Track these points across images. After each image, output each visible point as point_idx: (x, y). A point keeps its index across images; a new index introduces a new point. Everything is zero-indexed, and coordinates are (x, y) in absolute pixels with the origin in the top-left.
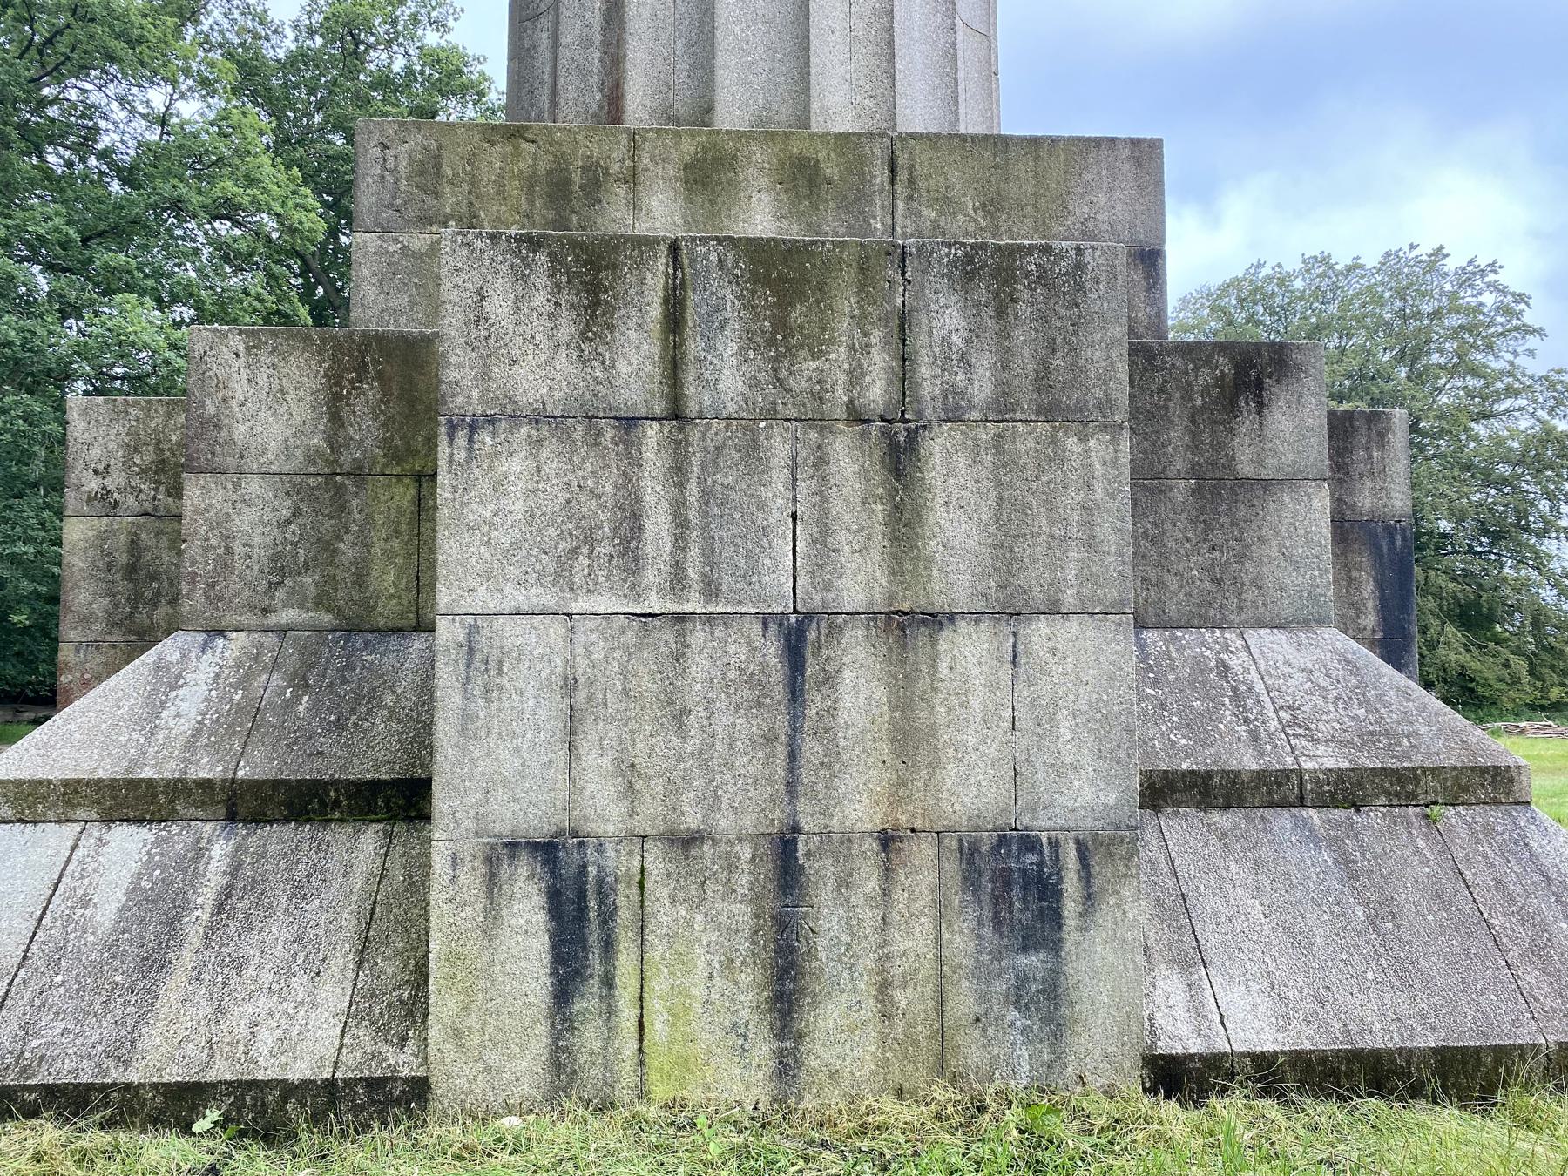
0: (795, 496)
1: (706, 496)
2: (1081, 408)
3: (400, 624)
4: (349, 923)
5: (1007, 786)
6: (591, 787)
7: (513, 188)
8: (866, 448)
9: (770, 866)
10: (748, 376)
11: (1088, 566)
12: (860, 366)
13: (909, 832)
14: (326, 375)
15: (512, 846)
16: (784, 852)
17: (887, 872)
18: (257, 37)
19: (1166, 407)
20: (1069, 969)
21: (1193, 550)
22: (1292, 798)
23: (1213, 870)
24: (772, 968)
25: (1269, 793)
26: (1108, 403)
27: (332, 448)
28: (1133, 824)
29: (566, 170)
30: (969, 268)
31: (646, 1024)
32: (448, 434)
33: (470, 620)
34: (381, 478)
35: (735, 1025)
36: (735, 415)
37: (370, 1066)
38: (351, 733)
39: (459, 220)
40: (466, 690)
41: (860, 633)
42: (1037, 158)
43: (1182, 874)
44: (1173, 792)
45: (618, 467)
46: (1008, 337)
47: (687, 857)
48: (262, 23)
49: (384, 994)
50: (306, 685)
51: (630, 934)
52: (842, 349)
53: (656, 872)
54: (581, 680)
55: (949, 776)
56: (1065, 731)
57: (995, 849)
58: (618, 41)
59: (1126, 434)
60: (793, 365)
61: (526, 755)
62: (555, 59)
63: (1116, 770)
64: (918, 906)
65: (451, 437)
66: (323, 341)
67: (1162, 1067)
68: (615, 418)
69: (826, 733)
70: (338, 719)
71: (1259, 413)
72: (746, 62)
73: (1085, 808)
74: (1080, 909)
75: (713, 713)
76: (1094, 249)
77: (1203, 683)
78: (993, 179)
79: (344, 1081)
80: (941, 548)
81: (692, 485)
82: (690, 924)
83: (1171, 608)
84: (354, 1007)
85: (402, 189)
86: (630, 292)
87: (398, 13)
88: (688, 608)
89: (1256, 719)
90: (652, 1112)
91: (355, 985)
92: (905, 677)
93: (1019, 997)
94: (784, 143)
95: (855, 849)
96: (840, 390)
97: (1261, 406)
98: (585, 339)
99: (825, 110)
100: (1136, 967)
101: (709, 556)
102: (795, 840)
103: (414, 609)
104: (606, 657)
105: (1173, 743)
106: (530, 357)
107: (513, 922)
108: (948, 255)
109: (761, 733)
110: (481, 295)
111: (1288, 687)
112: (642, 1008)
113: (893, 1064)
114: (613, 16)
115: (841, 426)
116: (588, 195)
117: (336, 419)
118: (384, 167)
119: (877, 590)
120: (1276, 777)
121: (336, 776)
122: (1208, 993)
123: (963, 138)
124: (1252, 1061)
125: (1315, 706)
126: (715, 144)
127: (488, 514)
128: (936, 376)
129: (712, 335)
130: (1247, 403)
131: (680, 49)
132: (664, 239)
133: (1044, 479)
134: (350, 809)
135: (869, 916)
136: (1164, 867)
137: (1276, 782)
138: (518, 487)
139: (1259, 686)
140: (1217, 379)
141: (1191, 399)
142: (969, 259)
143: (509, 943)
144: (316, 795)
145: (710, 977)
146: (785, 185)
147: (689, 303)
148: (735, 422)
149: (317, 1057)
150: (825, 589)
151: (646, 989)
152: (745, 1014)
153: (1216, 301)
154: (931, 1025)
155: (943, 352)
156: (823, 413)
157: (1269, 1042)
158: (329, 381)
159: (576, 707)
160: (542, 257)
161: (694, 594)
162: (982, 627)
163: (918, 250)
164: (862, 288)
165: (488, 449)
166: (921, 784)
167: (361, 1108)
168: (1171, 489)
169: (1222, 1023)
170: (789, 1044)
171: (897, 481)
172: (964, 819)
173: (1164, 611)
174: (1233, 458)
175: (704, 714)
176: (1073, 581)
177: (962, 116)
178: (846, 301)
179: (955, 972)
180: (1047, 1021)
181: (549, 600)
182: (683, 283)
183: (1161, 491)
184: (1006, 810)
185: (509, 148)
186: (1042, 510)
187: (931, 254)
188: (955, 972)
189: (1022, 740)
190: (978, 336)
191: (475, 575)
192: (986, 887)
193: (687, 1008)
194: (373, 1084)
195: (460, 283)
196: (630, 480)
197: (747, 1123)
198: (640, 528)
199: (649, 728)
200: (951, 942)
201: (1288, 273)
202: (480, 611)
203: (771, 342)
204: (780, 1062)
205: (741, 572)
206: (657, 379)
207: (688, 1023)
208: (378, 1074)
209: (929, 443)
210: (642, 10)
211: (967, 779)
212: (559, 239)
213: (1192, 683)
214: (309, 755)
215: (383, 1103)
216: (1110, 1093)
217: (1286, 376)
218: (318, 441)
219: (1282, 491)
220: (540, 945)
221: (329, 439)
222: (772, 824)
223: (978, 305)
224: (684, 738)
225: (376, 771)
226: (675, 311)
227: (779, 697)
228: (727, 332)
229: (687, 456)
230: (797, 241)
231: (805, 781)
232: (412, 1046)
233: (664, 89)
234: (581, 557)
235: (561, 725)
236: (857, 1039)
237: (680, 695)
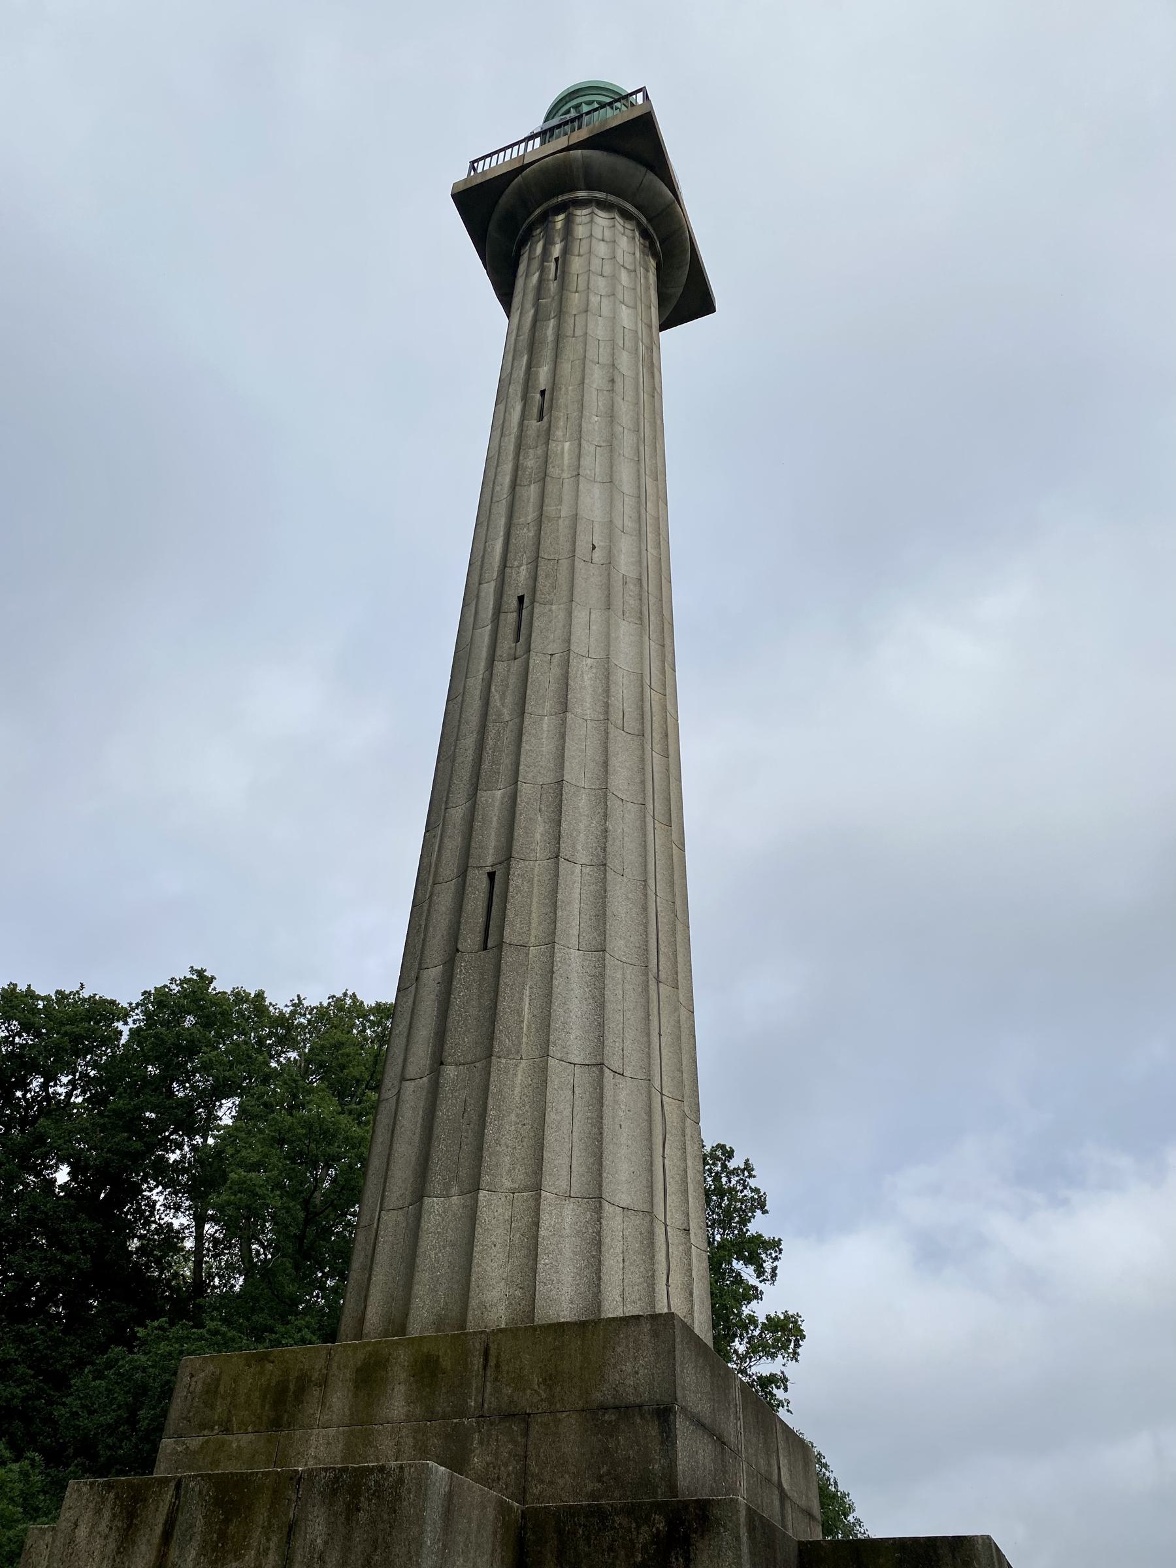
52: (253, 1552)
85: (196, 1404)
98: (118, 1552)
99: (483, 1306)
108: (324, 1478)
118: (189, 1392)
129: (184, 1546)
130: (677, 1559)
182: (177, 1509)
210: (385, 1246)
223: (335, 1515)
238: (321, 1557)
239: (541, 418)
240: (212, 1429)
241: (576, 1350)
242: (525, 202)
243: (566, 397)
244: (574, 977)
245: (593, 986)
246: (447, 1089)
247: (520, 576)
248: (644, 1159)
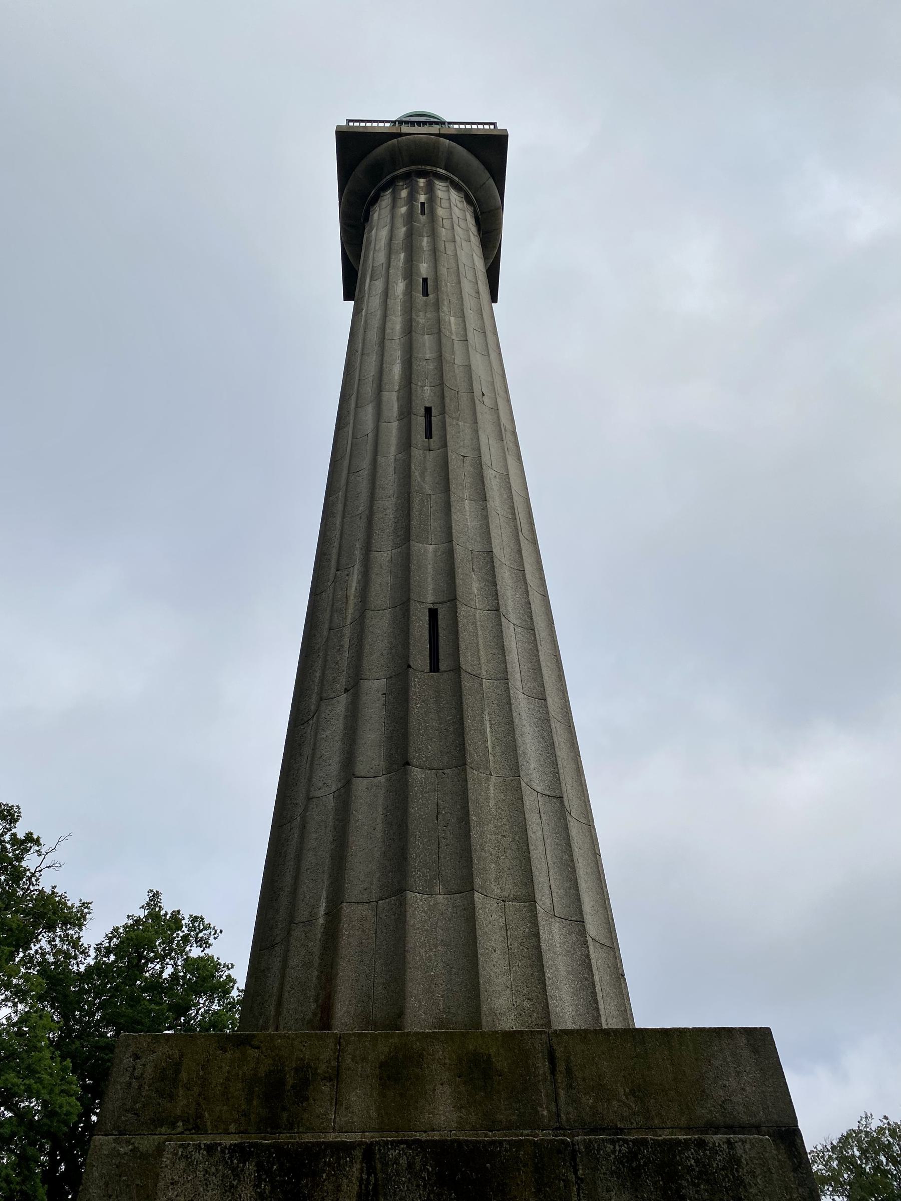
18: (67, 956)
30: (634, 1165)
39: (186, 1121)
62: (283, 977)
76: (744, 1142)
108: (614, 1152)
118: (132, 1076)
123: (607, 1032)
142: (633, 1156)
160: (250, 1167)
163: (586, 1148)
177: (602, 1012)
187: (598, 1151)
239: (426, 293)
240: (173, 1125)
241: (663, 1059)
242: (394, 159)
243: (448, 286)
244: (524, 715)
245: (540, 727)
246: (416, 788)
247: (426, 394)
248: (598, 897)
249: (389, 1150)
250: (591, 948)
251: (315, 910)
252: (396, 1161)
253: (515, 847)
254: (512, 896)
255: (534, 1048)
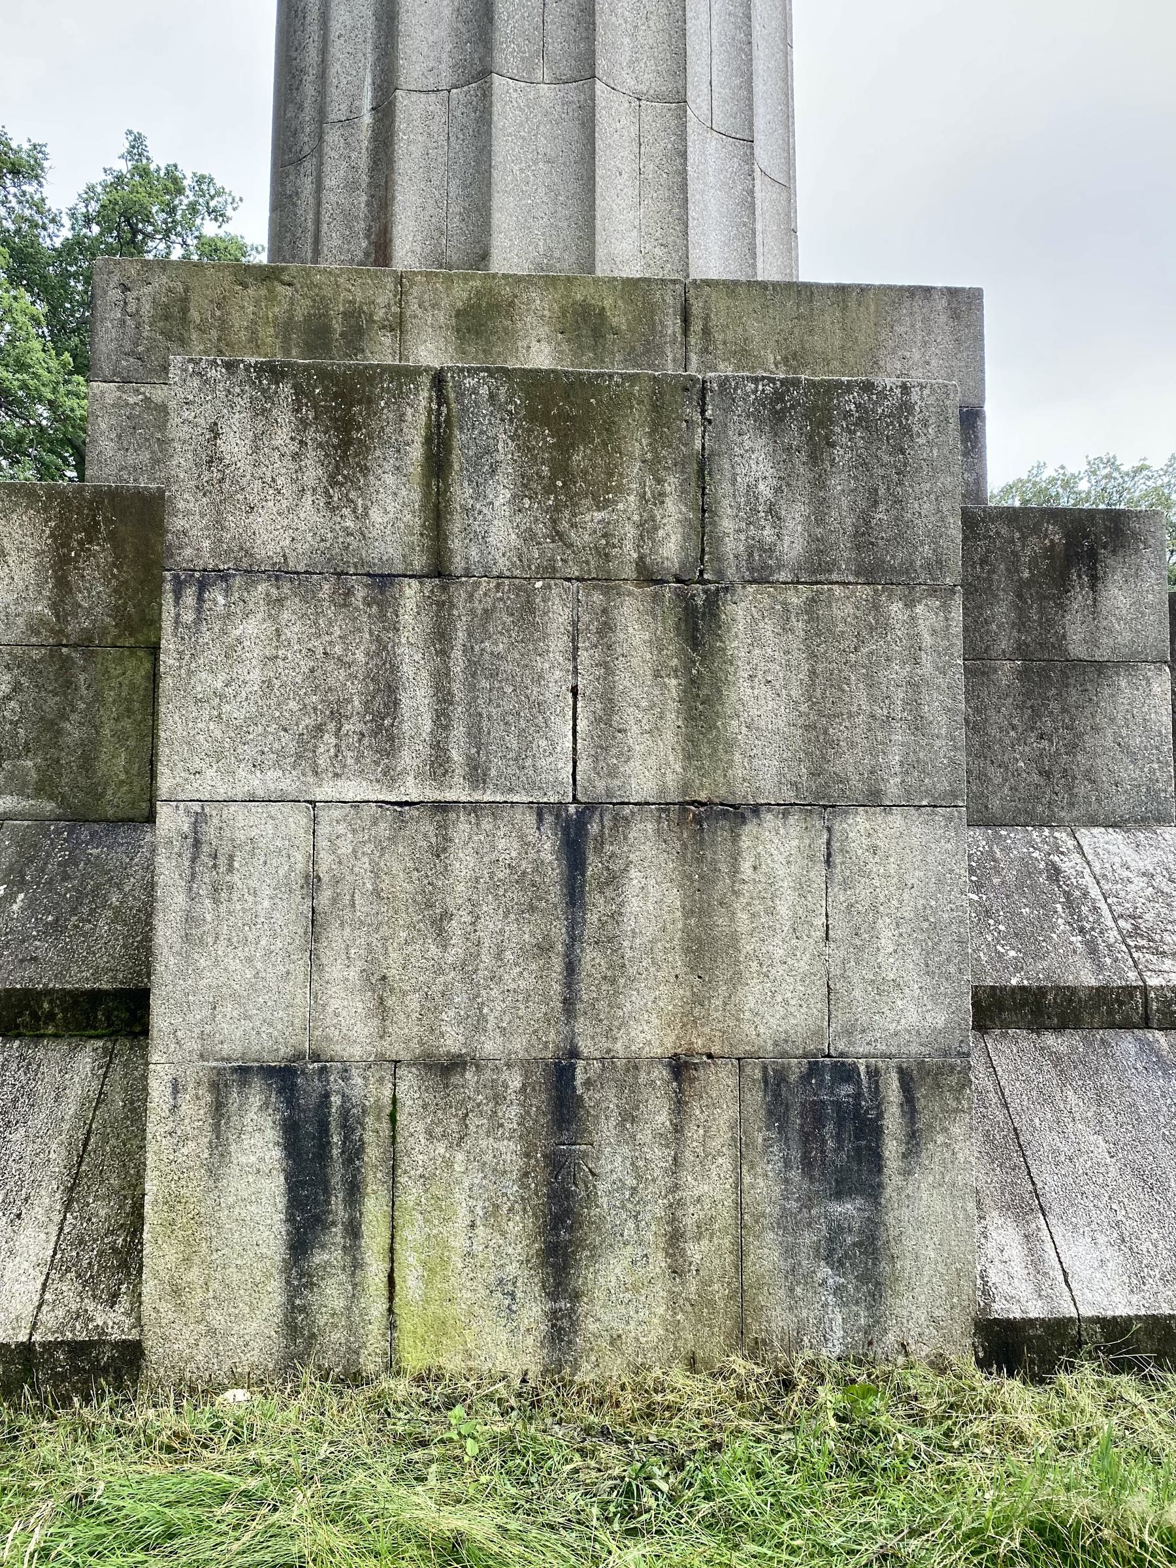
0: (575, 667)
1: (473, 667)
2: (907, 569)
3: (131, 814)
4: (57, 1156)
5: (819, 1006)
6: (335, 1004)
7: (267, 334)
8: (659, 612)
9: (544, 1096)
10: (523, 527)
11: (915, 752)
12: (652, 518)
13: (705, 1058)
14: (52, 535)
15: (243, 1072)
16: (559, 1079)
17: (680, 1106)
19: (989, 580)
20: (890, 1219)
21: (1019, 739)
22: (1136, 1019)
23: (1049, 1100)
24: (545, 1216)
25: (1110, 1012)
26: (938, 564)
27: (57, 616)
28: (965, 1050)
29: (326, 315)
30: (778, 407)
31: (397, 1280)
32: (174, 591)
33: (196, 807)
34: (112, 650)
35: (501, 1281)
36: (508, 574)
37: (73, 1329)
38: (70, 936)
40: (190, 889)
41: (649, 826)
42: (845, 309)
43: (1014, 1105)
44: (1001, 1010)
45: (371, 633)
46: (823, 487)
47: (447, 1086)
48: (38, 212)
49: (95, 1240)
50: (23, 882)
51: (379, 1175)
52: (632, 498)
53: (410, 1103)
54: (325, 878)
55: (751, 995)
56: (887, 941)
57: (805, 1078)
58: (386, 182)
59: (958, 600)
60: (575, 515)
61: (259, 965)
62: (319, 204)
63: (945, 987)
64: (716, 1144)
65: (178, 596)
66: (50, 497)
67: (998, 1333)
68: (368, 575)
69: (609, 942)
70: (57, 920)
71: (1093, 587)
72: (526, 205)
73: (909, 1032)
74: (903, 1149)
75: (478, 917)
77: (1032, 888)
78: (796, 330)
79: (42, 1345)
80: (744, 730)
81: (457, 653)
82: (449, 1164)
83: (995, 804)
84: (58, 1256)
85: (145, 334)
86: (388, 430)
87: (177, 202)
88: (450, 796)
89: (1093, 929)
90: (401, 1388)
91: (61, 1229)
92: (702, 877)
93: (831, 1251)
94: (566, 289)
95: (643, 1077)
96: (628, 546)
97: (1094, 580)
98: (333, 482)
100: (967, 1217)
101: (475, 736)
102: (573, 1067)
103: (147, 797)
104: (354, 851)
105: (1000, 956)
106: (271, 504)
107: (243, 1160)
108: (755, 392)
109: (534, 941)
110: (215, 432)
111: (1127, 893)
112: (392, 1261)
113: (684, 1329)
114: (382, 155)
115: (630, 587)
116: (349, 343)
117: (63, 585)
118: (124, 311)
119: (670, 777)
120: (1118, 994)
121: (51, 986)
122: (1049, 1246)
123: (764, 286)
124: (1102, 1328)
125: (1158, 915)
126: (491, 289)
127: (219, 685)
128: (739, 531)
130: (1079, 577)
131: (454, 190)
132: (427, 369)
133: (865, 650)
134: (66, 1022)
135: (659, 1156)
136: (993, 1098)
137: (1117, 1000)
138: (253, 653)
139: (1094, 892)
140: (1046, 549)
141: (1018, 571)
142: (778, 397)
143: (236, 1185)
144: (27, 1006)
145: (473, 1226)
146: (567, 335)
147: (455, 444)
148: (507, 582)
149: (13, 1316)
150: (609, 775)
151: (397, 1239)
152: (512, 1269)
153: (1008, 490)
154: (729, 1284)
155: (748, 503)
156: (609, 572)
157: (1121, 1306)
158: (55, 542)
159: (319, 909)
160: (286, 389)
161: (458, 779)
162: (792, 820)
163: (720, 386)
164: (655, 428)
165: (220, 609)
166: (719, 1002)
167: (63, 1377)
168: (995, 671)
169: (1066, 1281)
170: (564, 1304)
171: (694, 650)
172: (770, 1042)
173: (986, 807)
174: (1064, 637)
175: (468, 919)
176: (898, 769)
178: (637, 443)
179: (757, 1222)
180: (863, 1279)
181: (288, 784)
183: (983, 673)
184: (818, 1033)
185: (263, 292)
186: (861, 686)
187: (735, 389)
188: (757, 1222)
189: (836, 952)
190: (788, 485)
191: (203, 755)
192: (794, 1123)
193: (444, 1262)
194: (77, 1349)
195: (191, 418)
196: (385, 648)
197: (513, 1402)
198: (396, 703)
199: (403, 935)
200: (752, 1186)
201: (1073, 475)
202: (208, 797)
203: (550, 489)
204: (553, 1326)
205: (511, 755)
206: (417, 530)
207: (446, 1279)
208: (83, 1337)
209: (730, 607)
210: (412, 148)
211: (773, 997)
212: (306, 368)
213: (1020, 887)
214: (22, 961)
215: (89, 1371)
216: (940, 1366)
217: (1123, 546)
218: (42, 608)
219: (1118, 675)
220: (274, 1187)
221: (54, 606)
222: (546, 1047)
223: (788, 449)
224: (444, 946)
225: (97, 980)
226: (439, 452)
227: (556, 900)
228: (499, 477)
229: (451, 621)
230: (580, 374)
231: (585, 997)
232: (124, 1302)
233: (436, 234)
234: (326, 736)
235: (301, 931)
236: (643, 1299)
237: (440, 896)
238: (771, 510)
249: (465, 377)
250: (758, 182)
251: (357, 103)
252: (475, 391)
253: (664, 11)
254: (652, 92)
255: (664, 300)
